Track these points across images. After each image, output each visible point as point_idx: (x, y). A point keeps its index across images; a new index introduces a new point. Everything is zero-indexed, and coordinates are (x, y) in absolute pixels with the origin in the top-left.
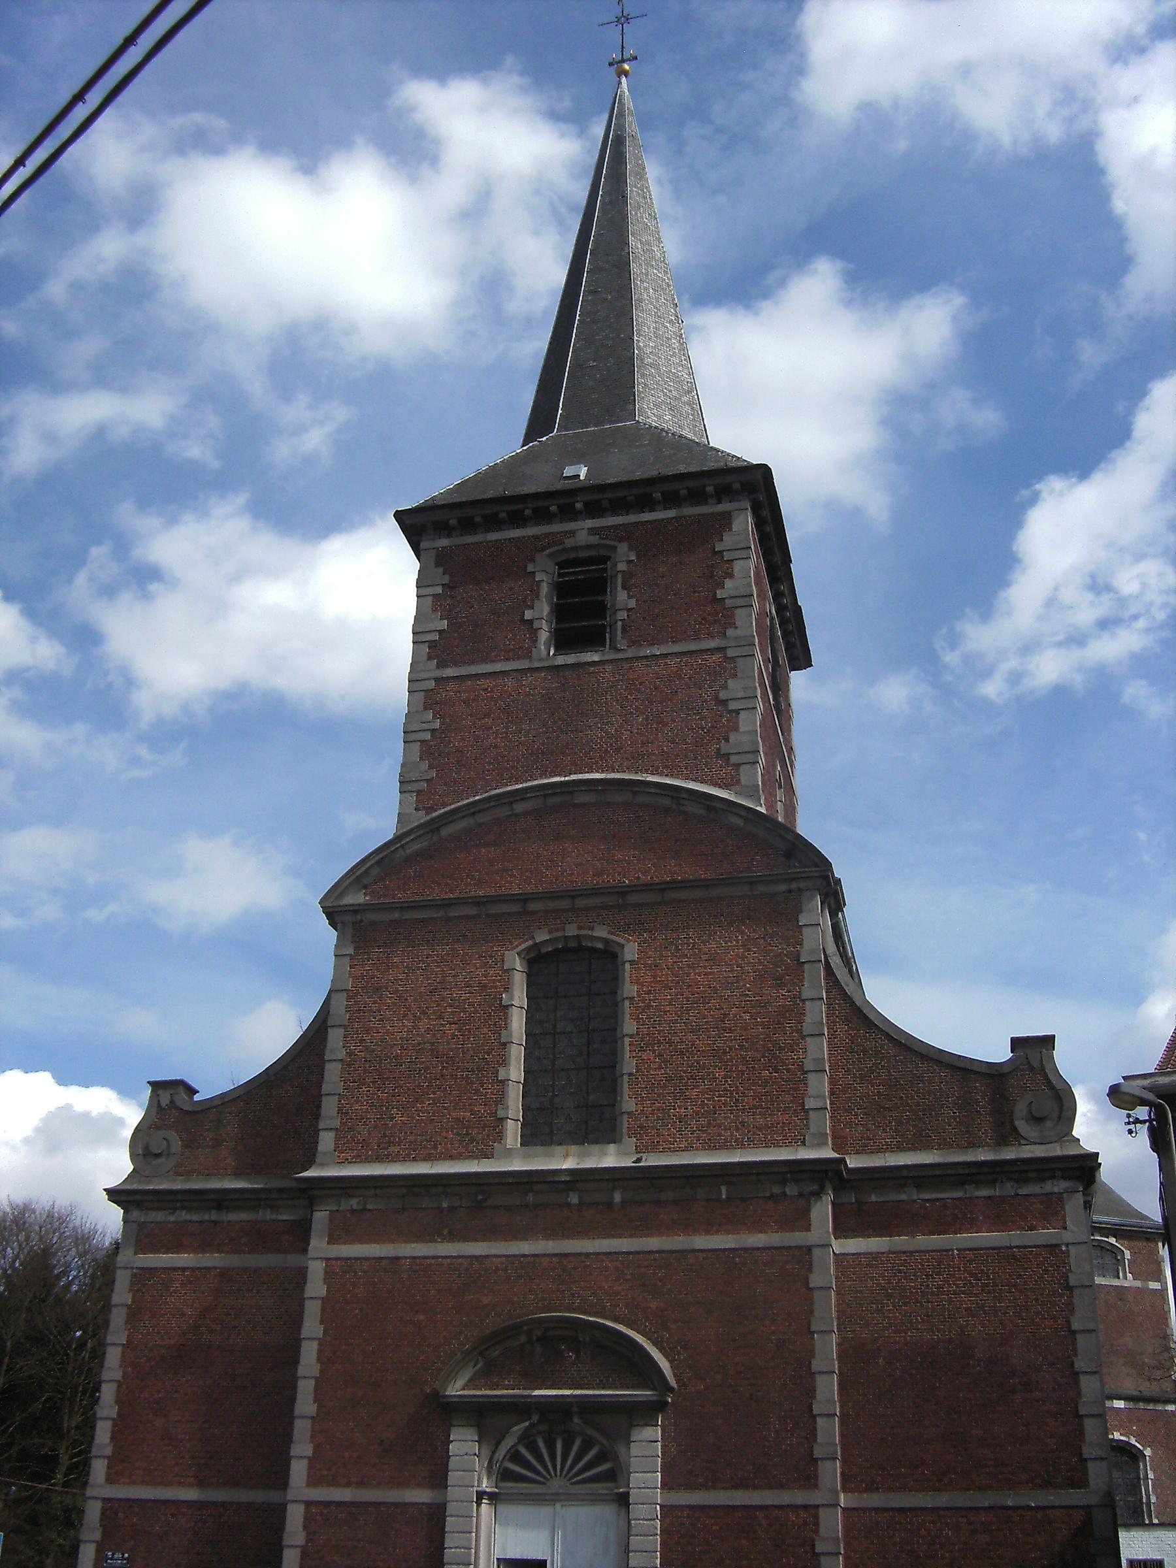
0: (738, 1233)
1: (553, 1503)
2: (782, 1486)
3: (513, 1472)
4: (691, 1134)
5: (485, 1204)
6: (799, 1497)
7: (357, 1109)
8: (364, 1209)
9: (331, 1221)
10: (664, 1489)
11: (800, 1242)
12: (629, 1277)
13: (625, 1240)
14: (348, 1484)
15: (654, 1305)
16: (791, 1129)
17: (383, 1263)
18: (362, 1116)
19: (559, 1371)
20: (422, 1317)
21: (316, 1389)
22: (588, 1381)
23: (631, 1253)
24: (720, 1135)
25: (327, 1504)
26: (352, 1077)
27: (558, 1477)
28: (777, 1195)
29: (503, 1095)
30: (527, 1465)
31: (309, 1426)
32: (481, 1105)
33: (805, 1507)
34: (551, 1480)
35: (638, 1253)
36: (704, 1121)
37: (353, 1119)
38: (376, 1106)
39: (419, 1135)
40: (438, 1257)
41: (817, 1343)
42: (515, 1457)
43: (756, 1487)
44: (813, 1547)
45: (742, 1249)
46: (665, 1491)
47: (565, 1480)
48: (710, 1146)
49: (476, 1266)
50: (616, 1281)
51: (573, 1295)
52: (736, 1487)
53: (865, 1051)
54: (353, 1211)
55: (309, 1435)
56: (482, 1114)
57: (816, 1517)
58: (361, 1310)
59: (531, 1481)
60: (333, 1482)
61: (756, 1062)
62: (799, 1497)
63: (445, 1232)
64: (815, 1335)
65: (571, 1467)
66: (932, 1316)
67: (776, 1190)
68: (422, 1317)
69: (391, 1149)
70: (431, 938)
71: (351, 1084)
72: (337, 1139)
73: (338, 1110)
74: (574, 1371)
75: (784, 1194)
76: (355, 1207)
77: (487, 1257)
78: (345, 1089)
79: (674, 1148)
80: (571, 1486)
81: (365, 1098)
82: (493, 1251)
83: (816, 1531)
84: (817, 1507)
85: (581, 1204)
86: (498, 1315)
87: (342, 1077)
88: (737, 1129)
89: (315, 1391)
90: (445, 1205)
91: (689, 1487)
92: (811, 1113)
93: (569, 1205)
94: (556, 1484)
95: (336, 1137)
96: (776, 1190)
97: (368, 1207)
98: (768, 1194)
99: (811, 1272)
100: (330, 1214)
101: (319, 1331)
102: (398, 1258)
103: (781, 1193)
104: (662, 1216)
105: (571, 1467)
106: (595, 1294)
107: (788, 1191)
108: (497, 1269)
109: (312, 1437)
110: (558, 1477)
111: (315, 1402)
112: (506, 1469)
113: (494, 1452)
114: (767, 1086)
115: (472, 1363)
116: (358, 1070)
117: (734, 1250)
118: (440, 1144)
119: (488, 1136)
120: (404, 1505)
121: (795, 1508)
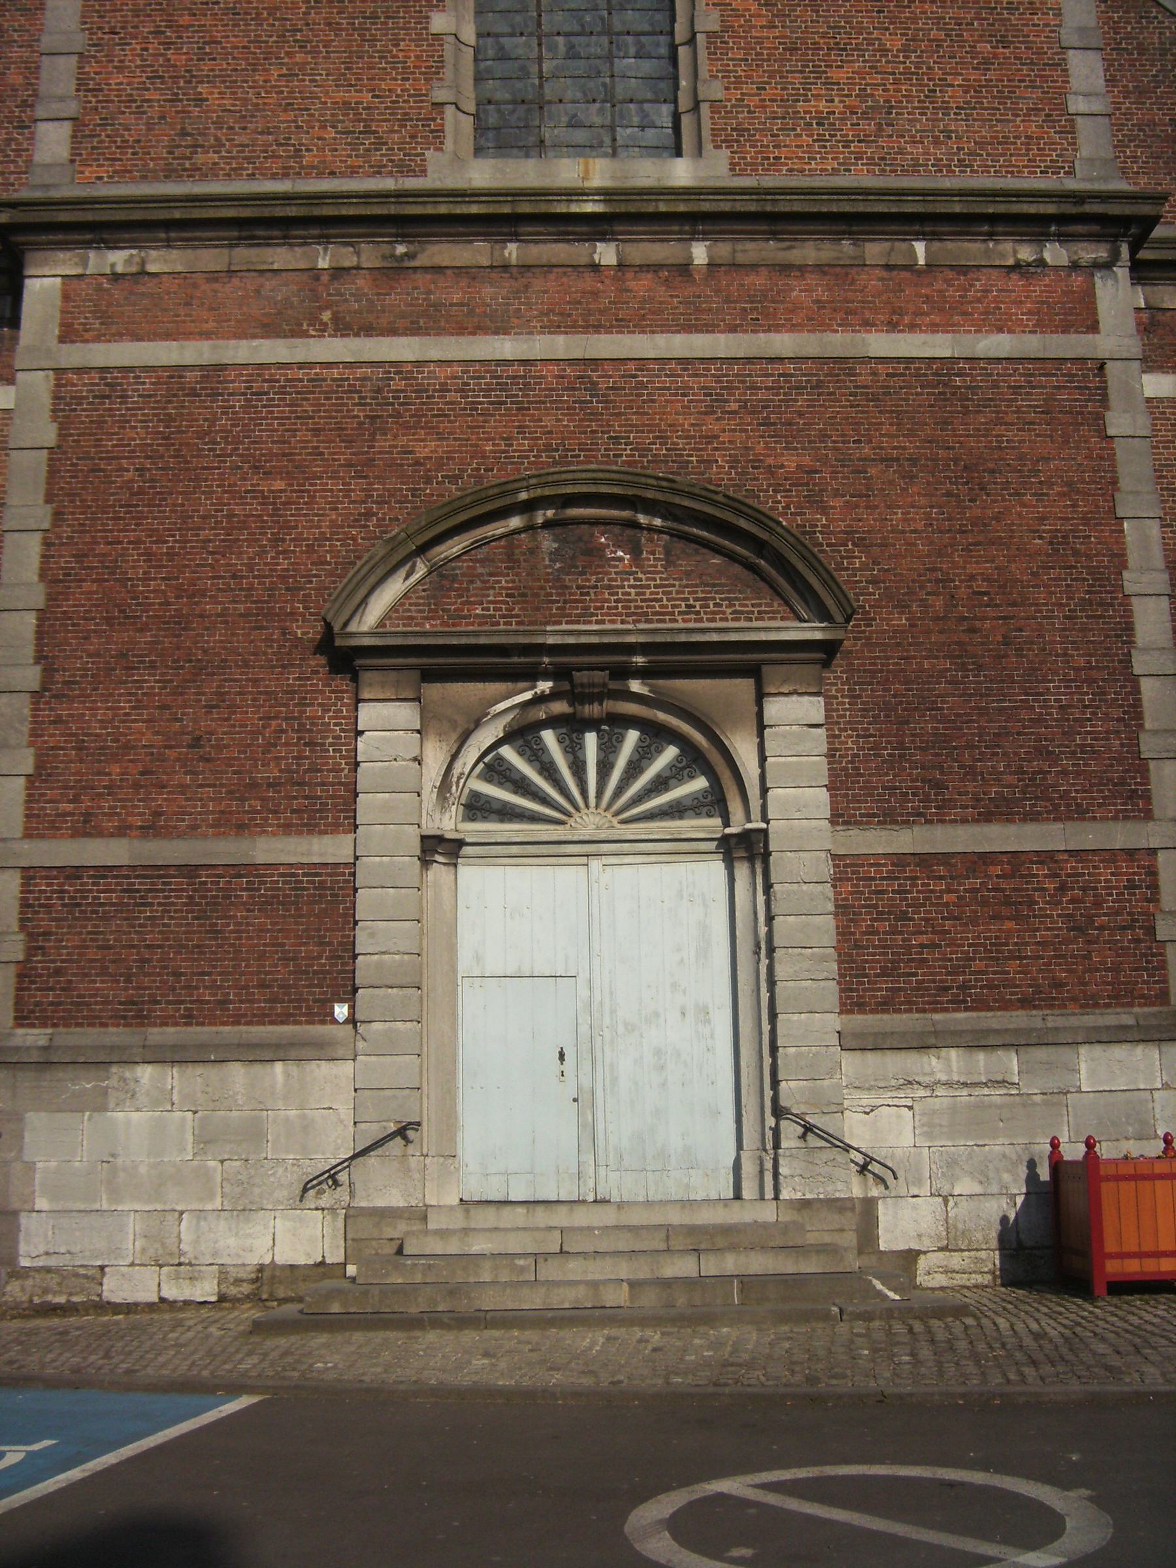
0: (954, 332)
1: (584, 860)
2: (1080, 813)
3: (489, 800)
4: (843, 147)
5: (413, 264)
6: (1121, 835)
7: (121, 84)
8: (143, 273)
9: (66, 297)
10: (838, 824)
11: (1081, 352)
12: (734, 406)
13: (722, 337)
14: (122, 831)
15: (790, 462)
16: (1044, 149)
17: (189, 376)
18: (131, 95)
19: (596, 587)
20: (279, 484)
21: (40, 634)
22: (661, 606)
23: (736, 359)
24: (901, 151)
25: (74, 872)
26: (109, 22)
27: (592, 810)
28: (1029, 265)
29: (442, 62)
30: (522, 786)
31: (27, 711)
32: (396, 79)
33: (1130, 853)
34: (576, 815)
35: (749, 360)
36: (869, 125)
37: (112, 101)
38: (161, 77)
39: (262, 133)
40: (311, 365)
41: (1128, 539)
42: (497, 771)
43: (1032, 817)
44: (1151, 930)
45: (967, 359)
46: (839, 828)
47: (609, 815)
48: (885, 171)
49: (397, 383)
50: (706, 413)
51: (616, 440)
52: (987, 817)
53: (1142, 49)
54: (116, 277)
55: (26, 729)
56: (397, 96)
57: (1153, 873)
58: (141, 470)
59: (534, 818)
60: (87, 828)
61: (964, 26)
62: (1121, 835)
63: (326, 316)
64: (1125, 525)
65: (619, 791)
66: (880, 710)
67: (1026, 253)
68: (279, 484)
69: (200, 158)
70: (317, 503)
71: (106, 37)
72: (76, 138)
73: (78, 85)
74: (630, 586)
75: (1041, 263)
76: (120, 269)
77: (418, 363)
78: (94, 45)
79: (810, 170)
80: (619, 826)
81: (139, 63)
82: (434, 354)
83: (1155, 899)
84: (1153, 851)
85: (621, 266)
86: (454, 479)
87: (86, 23)
88: (936, 142)
89: (37, 639)
90: (323, 263)
91: (889, 818)
92: (1079, 120)
93: (595, 267)
94: (589, 823)
95: (74, 137)
96: (1026, 253)
97: (152, 268)
98: (1011, 262)
99: (1107, 408)
100: (63, 284)
101: (42, 516)
102: (221, 367)
103: (1035, 261)
104: (795, 293)
105: (619, 791)
106: (663, 439)
107: (1047, 256)
108: (444, 389)
109: (34, 734)
110: (592, 810)
111: (37, 663)
112: (475, 795)
113: (454, 757)
114: (988, 69)
115: (402, 572)
116: (122, 10)
117: (953, 360)
118: (308, 150)
119: (413, 137)
120: (252, 868)
121: (1110, 856)
